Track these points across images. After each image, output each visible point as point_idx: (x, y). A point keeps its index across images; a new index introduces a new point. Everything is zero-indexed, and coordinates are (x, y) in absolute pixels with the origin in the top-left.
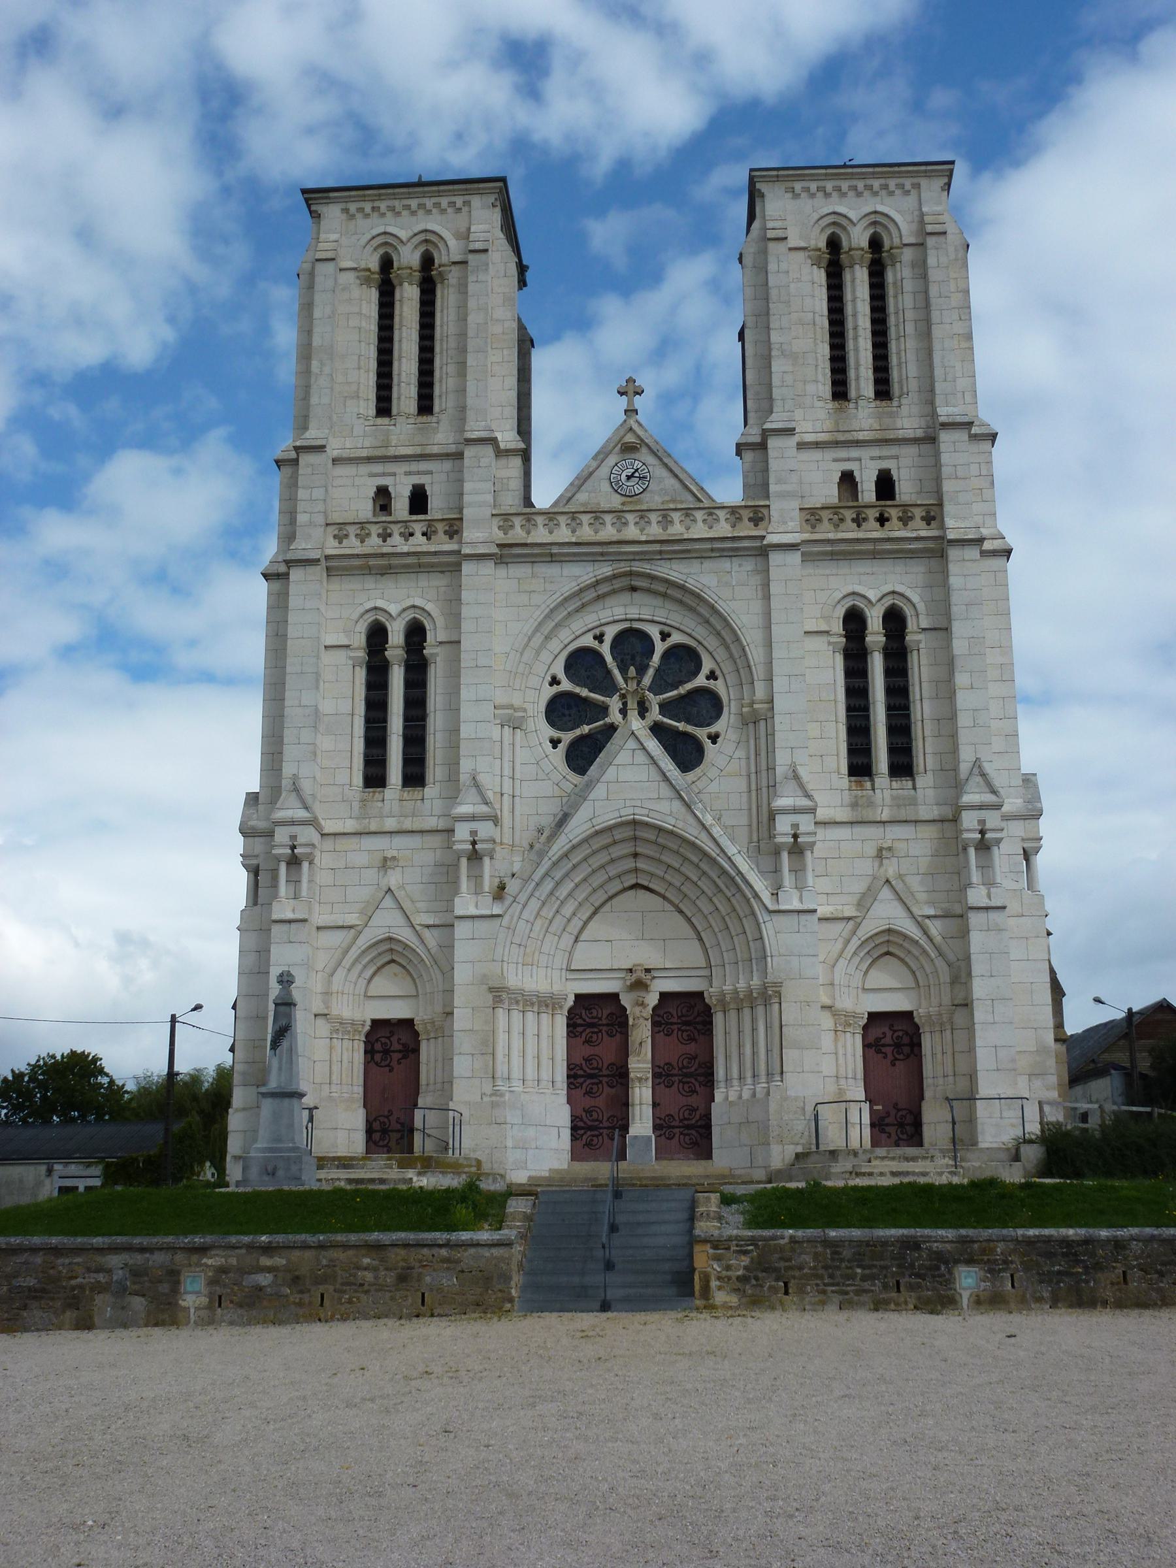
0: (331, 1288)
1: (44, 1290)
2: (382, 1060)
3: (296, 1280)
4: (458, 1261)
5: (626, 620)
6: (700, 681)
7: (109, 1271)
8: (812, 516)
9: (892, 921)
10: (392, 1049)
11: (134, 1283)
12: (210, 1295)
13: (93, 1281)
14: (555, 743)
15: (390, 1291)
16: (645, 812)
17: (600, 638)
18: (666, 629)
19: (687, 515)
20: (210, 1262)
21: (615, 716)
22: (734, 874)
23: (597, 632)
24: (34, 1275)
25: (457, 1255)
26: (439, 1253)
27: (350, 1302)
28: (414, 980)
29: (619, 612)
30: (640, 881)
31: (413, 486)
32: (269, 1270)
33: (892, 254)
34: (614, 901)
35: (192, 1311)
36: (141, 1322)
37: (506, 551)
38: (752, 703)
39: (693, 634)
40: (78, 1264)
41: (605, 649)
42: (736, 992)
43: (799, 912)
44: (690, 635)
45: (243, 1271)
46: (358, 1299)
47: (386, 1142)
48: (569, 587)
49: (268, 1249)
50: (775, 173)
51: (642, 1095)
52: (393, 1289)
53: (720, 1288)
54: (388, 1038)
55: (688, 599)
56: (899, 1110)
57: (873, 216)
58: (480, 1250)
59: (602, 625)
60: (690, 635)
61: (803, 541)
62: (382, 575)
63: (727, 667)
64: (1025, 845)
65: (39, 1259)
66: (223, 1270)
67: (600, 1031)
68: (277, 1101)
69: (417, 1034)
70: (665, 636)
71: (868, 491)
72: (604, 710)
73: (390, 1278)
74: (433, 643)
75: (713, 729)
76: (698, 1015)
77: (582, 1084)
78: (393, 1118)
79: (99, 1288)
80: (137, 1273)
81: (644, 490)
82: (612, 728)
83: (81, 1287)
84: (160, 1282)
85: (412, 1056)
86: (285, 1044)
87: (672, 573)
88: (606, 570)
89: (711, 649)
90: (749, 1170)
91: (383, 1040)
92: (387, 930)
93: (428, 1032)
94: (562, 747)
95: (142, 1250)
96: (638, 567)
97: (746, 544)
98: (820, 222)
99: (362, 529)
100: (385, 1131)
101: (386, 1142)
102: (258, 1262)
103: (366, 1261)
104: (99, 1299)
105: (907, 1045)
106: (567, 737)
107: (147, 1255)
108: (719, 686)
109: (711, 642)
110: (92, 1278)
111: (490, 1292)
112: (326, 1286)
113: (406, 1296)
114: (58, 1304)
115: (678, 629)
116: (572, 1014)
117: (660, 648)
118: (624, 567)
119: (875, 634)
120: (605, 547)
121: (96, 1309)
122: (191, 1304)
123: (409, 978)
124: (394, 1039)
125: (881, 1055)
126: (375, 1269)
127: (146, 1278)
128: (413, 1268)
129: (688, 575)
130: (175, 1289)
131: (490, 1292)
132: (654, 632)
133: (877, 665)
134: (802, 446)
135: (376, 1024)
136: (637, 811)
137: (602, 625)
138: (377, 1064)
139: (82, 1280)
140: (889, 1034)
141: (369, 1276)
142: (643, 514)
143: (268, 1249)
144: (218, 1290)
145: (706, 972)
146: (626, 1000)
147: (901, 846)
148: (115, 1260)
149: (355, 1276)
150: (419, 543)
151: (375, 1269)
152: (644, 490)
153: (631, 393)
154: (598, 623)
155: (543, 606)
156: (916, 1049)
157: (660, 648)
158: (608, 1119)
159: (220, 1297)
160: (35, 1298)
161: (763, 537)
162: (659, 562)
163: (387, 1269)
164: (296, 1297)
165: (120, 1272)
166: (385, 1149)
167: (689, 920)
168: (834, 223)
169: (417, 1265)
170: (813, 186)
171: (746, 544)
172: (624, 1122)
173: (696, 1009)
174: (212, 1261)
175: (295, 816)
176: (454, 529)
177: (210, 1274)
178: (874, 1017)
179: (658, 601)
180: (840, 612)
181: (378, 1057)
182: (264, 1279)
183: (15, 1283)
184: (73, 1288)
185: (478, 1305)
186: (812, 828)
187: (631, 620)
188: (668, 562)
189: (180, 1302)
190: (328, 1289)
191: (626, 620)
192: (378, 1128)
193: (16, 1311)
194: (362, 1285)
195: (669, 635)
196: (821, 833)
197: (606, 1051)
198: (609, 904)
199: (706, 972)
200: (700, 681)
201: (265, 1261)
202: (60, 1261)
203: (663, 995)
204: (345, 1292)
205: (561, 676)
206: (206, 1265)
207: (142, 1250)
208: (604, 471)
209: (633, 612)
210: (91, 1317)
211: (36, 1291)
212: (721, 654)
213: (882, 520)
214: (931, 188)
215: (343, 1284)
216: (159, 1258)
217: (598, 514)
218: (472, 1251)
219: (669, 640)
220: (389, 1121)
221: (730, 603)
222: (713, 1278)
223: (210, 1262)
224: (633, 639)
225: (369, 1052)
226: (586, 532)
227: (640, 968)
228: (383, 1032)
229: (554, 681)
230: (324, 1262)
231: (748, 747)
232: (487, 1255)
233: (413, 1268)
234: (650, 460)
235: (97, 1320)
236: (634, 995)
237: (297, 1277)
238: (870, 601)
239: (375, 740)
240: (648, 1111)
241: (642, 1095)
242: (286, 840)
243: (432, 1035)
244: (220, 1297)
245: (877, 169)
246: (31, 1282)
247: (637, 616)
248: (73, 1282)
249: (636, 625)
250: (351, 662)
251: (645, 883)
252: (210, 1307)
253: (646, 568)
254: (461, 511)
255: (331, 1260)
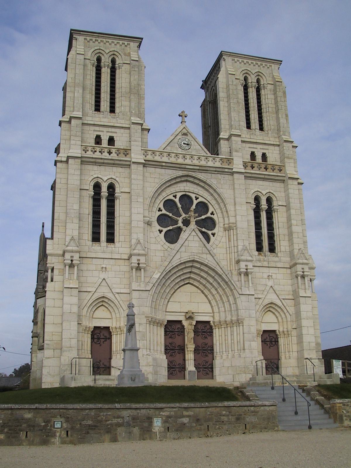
0: (211, 423)
1: (96, 426)
2: (97, 341)
3: (198, 420)
4: (257, 412)
5: (184, 191)
6: (209, 215)
7: (123, 418)
8: (245, 165)
9: (273, 300)
10: (101, 338)
11: (134, 423)
12: (164, 427)
13: (116, 422)
14: (161, 231)
15: (233, 424)
16: (198, 257)
17: (175, 196)
18: (198, 196)
19: (214, 159)
20: (163, 414)
21: (180, 224)
22: (228, 281)
23: (174, 194)
24: (91, 420)
25: (257, 409)
26: (251, 409)
27: (219, 429)
28: (111, 313)
29: (182, 189)
30: (190, 282)
31: (110, 136)
32: (188, 416)
33: (264, 86)
34: (181, 288)
35: (158, 433)
36: (138, 439)
37: (147, 162)
38: (229, 223)
39: (207, 199)
40: (109, 415)
41: (177, 200)
42: (232, 321)
43: (249, 295)
44: (206, 199)
45: (177, 417)
46: (222, 427)
47: (99, 372)
48: (168, 178)
49: (186, 408)
50: (229, 54)
51: (190, 356)
52: (235, 423)
53: (346, 420)
54: (99, 333)
55: (207, 187)
56: (272, 363)
57: (258, 73)
58: (265, 407)
59: (176, 192)
60: (206, 199)
61: (245, 172)
62: (100, 166)
63: (218, 211)
64: (311, 278)
65: (93, 413)
66: (169, 417)
67: (175, 334)
68: (132, 352)
69: (111, 333)
70: (197, 198)
71: (105, 142)
72: (176, 222)
73: (233, 419)
74: (119, 192)
75: (213, 232)
76: (208, 329)
77: (169, 352)
78: (101, 363)
79: (119, 425)
80: (134, 418)
81: (189, 149)
82: (180, 230)
83: (111, 424)
84: (144, 422)
85: (108, 341)
86: (133, 330)
87: (202, 177)
88: (180, 173)
89: (213, 205)
90: (233, 383)
91: (97, 334)
92: (103, 294)
93: (88, 331)
94: (163, 233)
95: (136, 409)
96: (191, 173)
97: (226, 170)
98: (242, 72)
99: (86, 148)
100: (98, 368)
101: (99, 372)
102: (183, 413)
103: (224, 412)
104: (119, 429)
105: (274, 342)
106: (165, 230)
107: (138, 411)
108: (215, 217)
109: (213, 202)
110: (115, 421)
111: (269, 423)
112: (209, 423)
113: (240, 426)
114: (102, 431)
115: (202, 197)
116: (166, 327)
117: (195, 202)
118: (185, 173)
119: (264, 204)
120: (181, 165)
121: (118, 434)
122: (157, 430)
123: (108, 312)
124: (101, 334)
125: (266, 345)
126: (228, 416)
127: (138, 421)
128: (242, 415)
129: (207, 178)
130: (151, 423)
131: (269, 423)
132: (193, 196)
133: (264, 216)
134: (243, 142)
135: (95, 328)
136: (195, 257)
137: (176, 192)
138: (95, 343)
139: (111, 422)
140: (268, 338)
141: (225, 419)
142: (192, 157)
143: (186, 408)
144: (168, 425)
145: (212, 315)
146: (185, 323)
147: (274, 276)
148: (125, 413)
149: (220, 418)
150: (97, 155)
151: (228, 416)
152: (189, 149)
153: (183, 116)
154: (175, 191)
155: (159, 183)
156: (277, 343)
157: (195, 202)
158: (178, 365)
159: (168, 427)
160: (92, 429)
161: (233, 169)
162: (197, 173)
163: (232, 415)
164: (198, 427)
165: (128, 418)
166: (99, 374)
167: (206, 296)
168: (246, 73)
169: (243, 414)
170: (240, 60)
171: (226, 170)
172: (184, 366)
173: (207, 327)
174: (165, 413)
175: (73, 249)
176: (126, 152)
177: (164, 419)
178: (265, 331)
179: (195, 186)
180: (92, 184)
181: (95, 340)
182: (185, 420)
183: (84, 423)
184: (108, 425)
185: (266, 428)
186: (252, 267)
187: (186, 192)
188: (201, 173)
189: (153, 430)
190: (211, 424)
191: (184, 191)
192: (96, 366)
193: (84, 435)
194: (223, 422)
195: (198, 198)
196: (256, 269)
197: (177, 341)
198: (179, 289)
199: (212, 315)
200: (209, 215)
201: (185, 413)
202: (102, 414)
203: (197, 322)
204: (217, 425)
205: (162, 208)
206: (162, 415)
207: (136, 409)
208: (176, 140)
209: (187, 189)
210: (116, 437)
211: (92, 426)
212: (216, 206)
213: (110, 153)
214: (274, 67)
215: (216, 422)
216: (143, 412)
217: (178, 154)
218: (262, 408)
219: (198, 200)
220: (100, 364)
221: (221, 190)
222: (344, 416)
223: (163, 414)
224: (186, 198)
225: (93, 338)
226: (173, 160)
227: (190, 312)
228: (97, 331)
229: (160, 210)
230: (208, 413)
231: (226, 238)
232: (268, 409)
233: (242, 415)
234: (191, 139)
235: (119, 438)
236: (188, 322)
237: (198, 419)
238: (263, 194)
239: (96, 225)
240: (192, 362)
241: (190, 356)
242: (69, 258)
243: (118, 333)
244: (168, 427)
245: (260, 59)
246: (90, 422)
247: (188, 191)
248: (108, 422)
249: (187, 193)
250: (88, 196)
251: (192, 282)
252: (164, 432)
253: (194, 174)
254: (130, 147)
255: (211, 413)
